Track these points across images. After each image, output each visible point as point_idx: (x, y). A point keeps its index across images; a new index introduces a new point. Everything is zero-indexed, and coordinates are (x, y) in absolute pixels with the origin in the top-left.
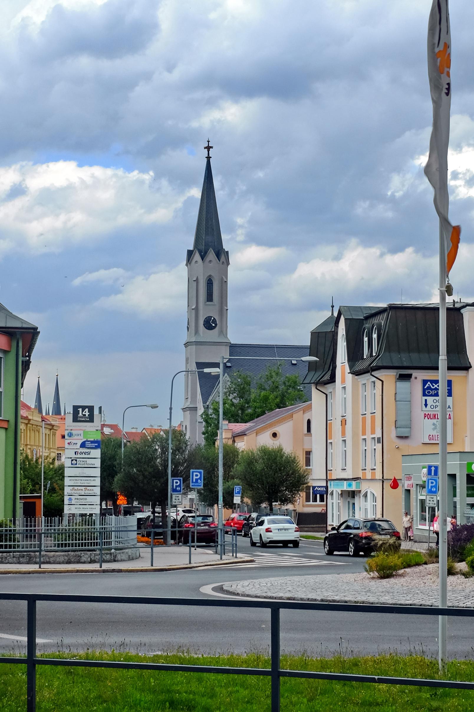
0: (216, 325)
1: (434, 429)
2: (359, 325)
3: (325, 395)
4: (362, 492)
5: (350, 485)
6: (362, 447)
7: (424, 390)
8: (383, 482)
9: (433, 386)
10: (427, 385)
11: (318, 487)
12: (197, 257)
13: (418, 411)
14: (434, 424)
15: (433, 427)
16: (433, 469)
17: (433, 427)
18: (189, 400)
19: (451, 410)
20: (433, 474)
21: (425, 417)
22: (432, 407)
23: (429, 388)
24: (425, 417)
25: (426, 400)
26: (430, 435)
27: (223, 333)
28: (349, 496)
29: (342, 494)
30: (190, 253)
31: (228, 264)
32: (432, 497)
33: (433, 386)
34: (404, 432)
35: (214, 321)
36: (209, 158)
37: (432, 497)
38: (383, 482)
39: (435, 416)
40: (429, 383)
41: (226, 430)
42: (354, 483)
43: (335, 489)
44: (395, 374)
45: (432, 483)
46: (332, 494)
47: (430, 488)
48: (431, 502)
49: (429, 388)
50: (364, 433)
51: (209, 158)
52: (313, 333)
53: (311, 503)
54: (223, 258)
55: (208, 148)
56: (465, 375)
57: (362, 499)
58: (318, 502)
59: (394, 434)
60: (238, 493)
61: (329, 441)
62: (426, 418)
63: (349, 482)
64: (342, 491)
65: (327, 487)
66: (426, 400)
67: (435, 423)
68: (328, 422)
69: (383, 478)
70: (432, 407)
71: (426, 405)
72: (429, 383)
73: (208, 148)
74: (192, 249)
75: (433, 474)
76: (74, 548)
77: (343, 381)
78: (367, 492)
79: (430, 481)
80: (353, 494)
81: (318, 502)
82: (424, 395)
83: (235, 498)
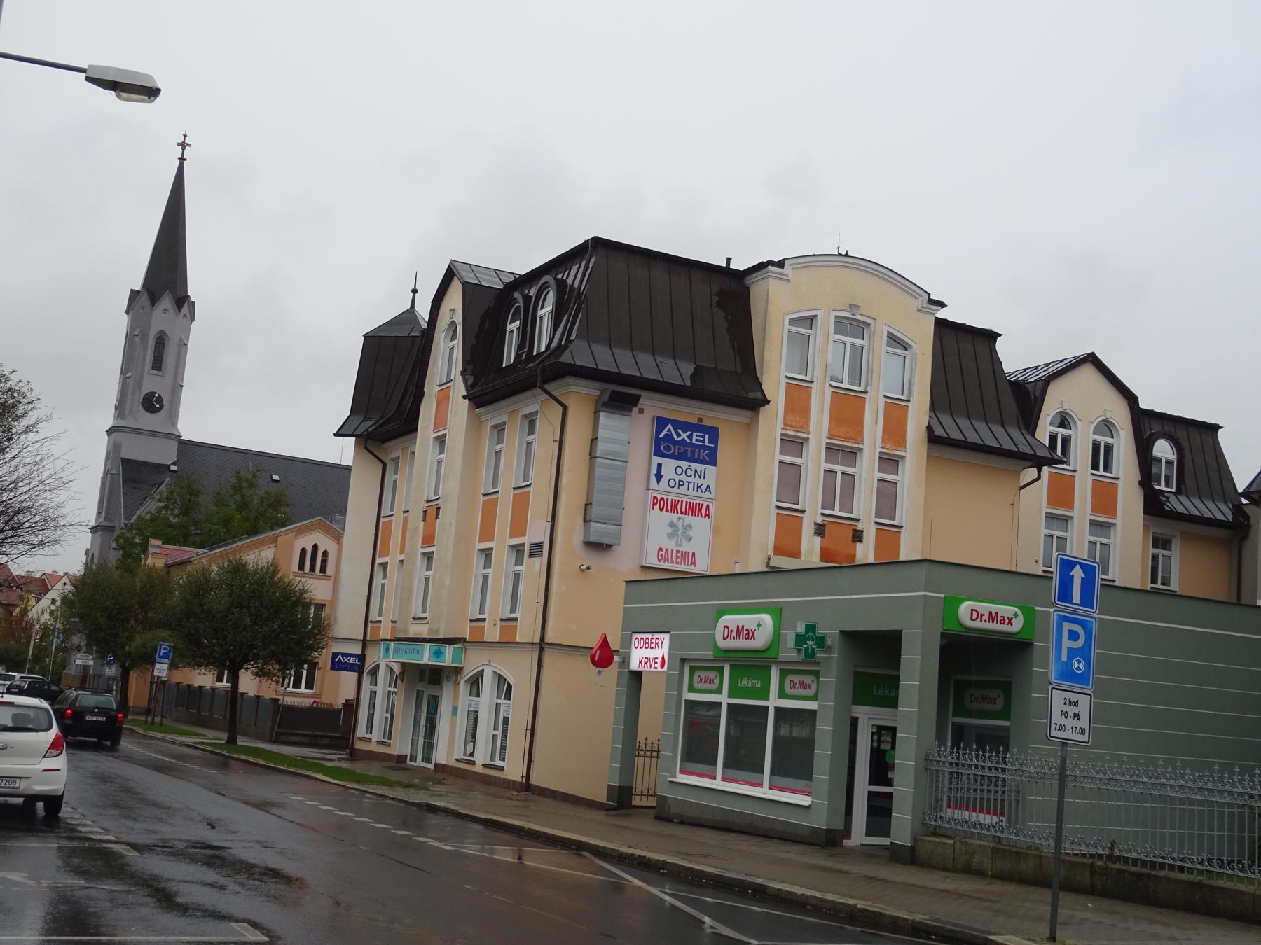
0: (162, 406)
1: (671, 536)
2: (491, 306)
3: (381, 466)
4: (465, 671)
5: (438, 654)
6: (478, 569)
7: (658, 442)
8: (542, 650)
9: (679, 435)
10: (665, 432)
11: (344, 655)
12: (144, 299)
13: (635, 492)
14: (672, 525)
15: (670, 530)
16: (1078, 573)
17: (670, 530)
18: (103, 515)
19: (712, 496)
20: (1076, 598)
21: (654, 504)
22: (672, 483)
23: (669, 438)
24: (654, 504)
25: (660, 465)
26: (660, 549)
27: (173, 417)
28: (421, 680)
29: (402, 673)
30: (134, 294)
31: (193, 319)
32: (1074, 697)
33: (679, 435)
34: (599, 531)
35: (160, 400)
36: (182, 159)
37: (1074, 697)
38: (542, 650)
39: (676, 506)
40: (670, 426)
41: (157, 556)
42: (448, 650)
43: (386, 660)
44: (597, 393)
45: (1073, 636)
46: (374, 672)
47: (1064, 658)
48: (1069, 723)
49: (669, 438)
50: (487, 534)
51: (182, 159)
52: (368, 338)
53: (291, 689)
54: (185, 309)
55: (184, 145)
56: (746, 420)
57: (463, 688)
58: (303, 690)
59: (578, 538)
60: (165, 656)
61: (378, 561)
62: (657, 507)
63: (436, 646)
64: (403, 665)
65: (362, 657)
66: (660, 465)
67: (675, 521)
68: (382, 520)
69: (542, 638)
70: (672, 483)
71: (659, 477)
72: (670, 426)
73: (184, 145)
74: (138, 289)
75: (1076, 598)
76: (1159, 586)
77: (440, 422)
78: (481, 674)
79: (1067, 627)
80: (435, 676)
81: (303, 690)
82: (658, 453)
83: (157, 666)
